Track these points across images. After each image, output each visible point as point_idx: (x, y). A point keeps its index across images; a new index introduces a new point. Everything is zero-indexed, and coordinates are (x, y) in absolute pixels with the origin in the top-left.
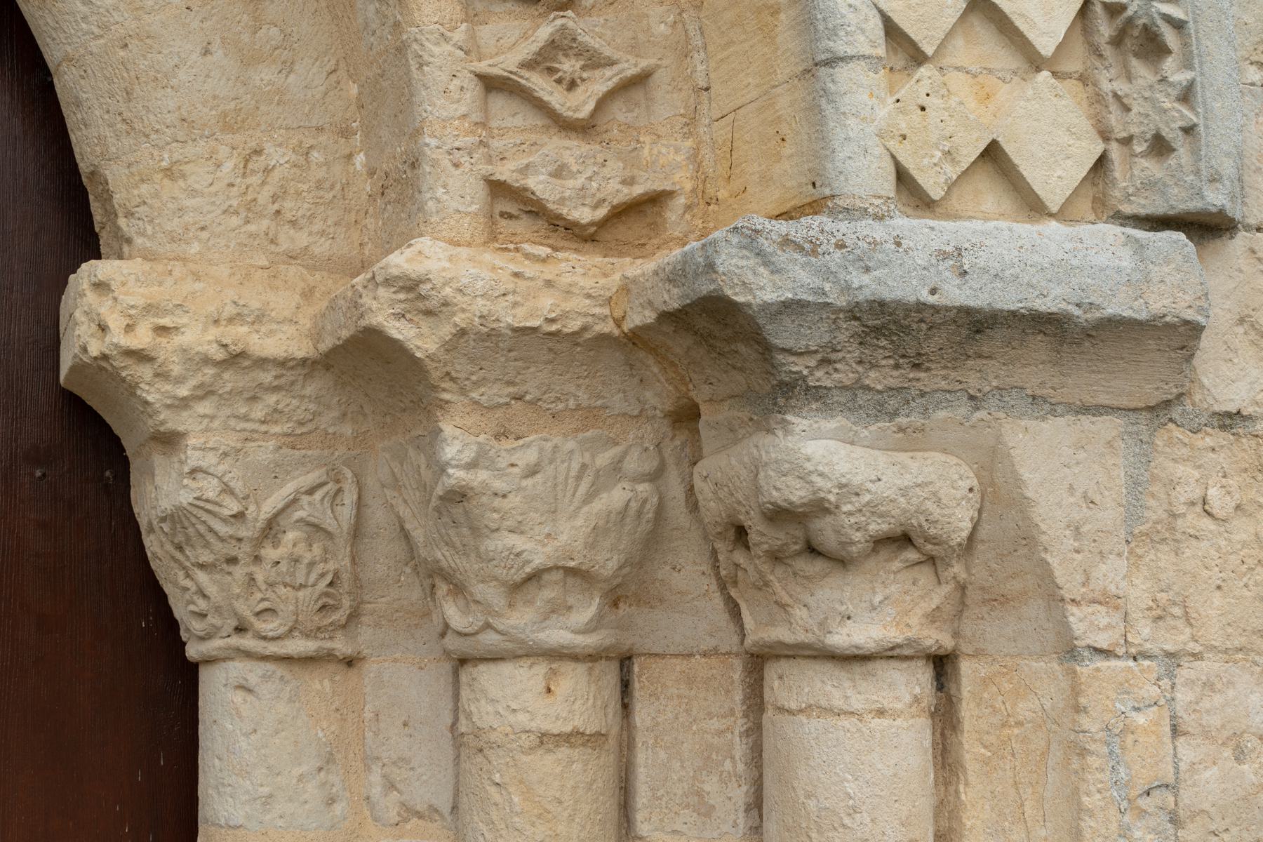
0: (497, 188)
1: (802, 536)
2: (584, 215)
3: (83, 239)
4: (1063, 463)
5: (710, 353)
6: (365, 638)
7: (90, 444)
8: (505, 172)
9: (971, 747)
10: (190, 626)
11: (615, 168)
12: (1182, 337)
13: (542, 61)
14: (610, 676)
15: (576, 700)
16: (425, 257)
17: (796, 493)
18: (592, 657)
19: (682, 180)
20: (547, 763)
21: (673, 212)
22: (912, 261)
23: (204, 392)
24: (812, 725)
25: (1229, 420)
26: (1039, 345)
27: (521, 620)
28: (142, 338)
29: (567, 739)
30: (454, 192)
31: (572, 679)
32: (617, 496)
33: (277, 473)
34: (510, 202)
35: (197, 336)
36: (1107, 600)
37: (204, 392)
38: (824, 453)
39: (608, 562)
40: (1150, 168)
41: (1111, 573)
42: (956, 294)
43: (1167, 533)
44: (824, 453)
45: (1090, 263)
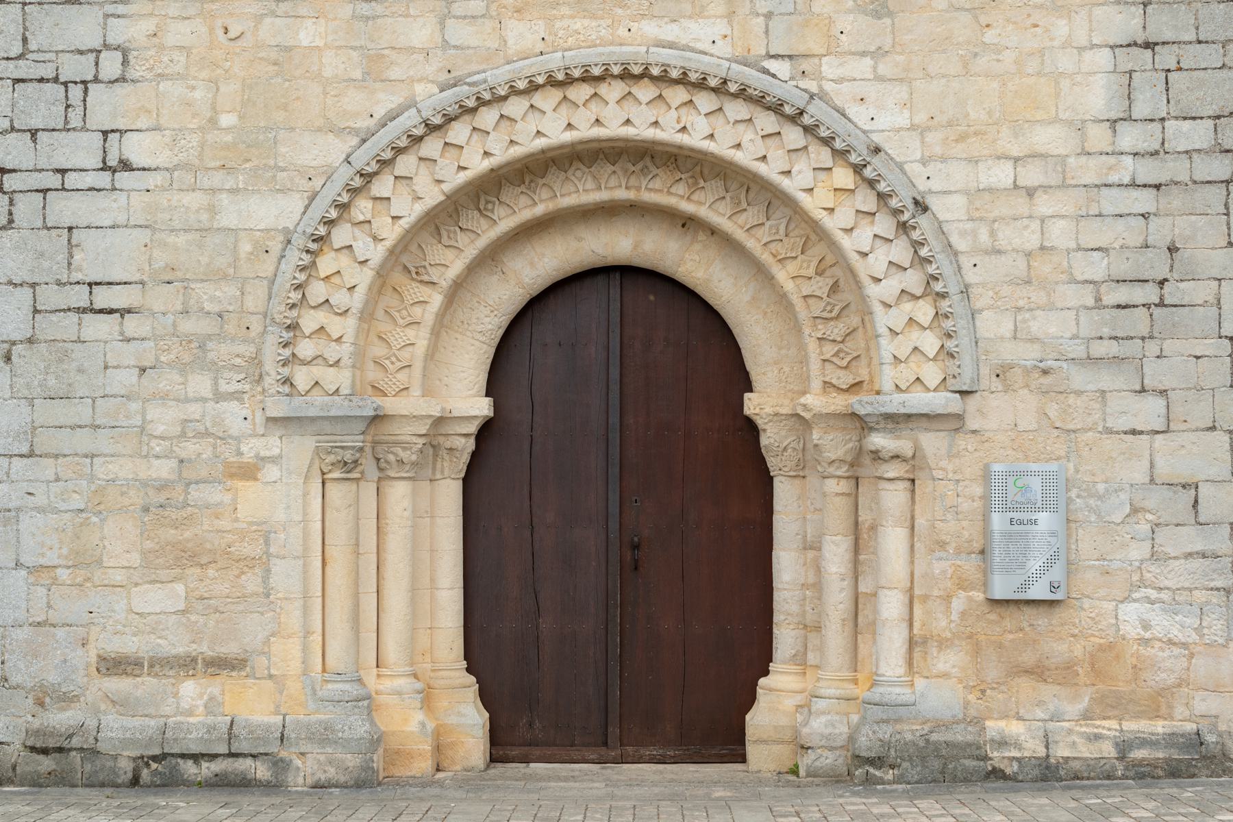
0: (825, 382)
1: (876, 455)
2: (844, 387)
3: (750, 389)
4: (932, 442)
5: (860, 423)
6: (807, 472)
7: (751, 429)
8: (827, 379)
9: (917, 498)
10: (771, 469)
11: (851, 376)
12: (959, 417)
13: (836, 354)
14: (853, 482)
15: (844, 486)
16: (808, 399)
17: (873, 448)
18: (848, 478)
19: (867, 378)
20: (838, 499)
21: (865, 385)
22: (894, 403)
23: (770, 421)
24: (883, 493)
25: (974, 432)
26: (924, 419)
27: (831, 470)
28: (757, 411)
29: (842, 494)
30: (816, 384)
31: (843, 482)
32: (850, 445)
33: (786, 437)
34: (828, 385)
35: (768, 410)
36: (941, 469)
37: (770, 421)
38: (879, 440)
39: (849, 459)
40: (953, 381)
41: (943, 464)
42: (903, 411)
43: (957, 455)
44: (879, 440)
45: (943, 402)
